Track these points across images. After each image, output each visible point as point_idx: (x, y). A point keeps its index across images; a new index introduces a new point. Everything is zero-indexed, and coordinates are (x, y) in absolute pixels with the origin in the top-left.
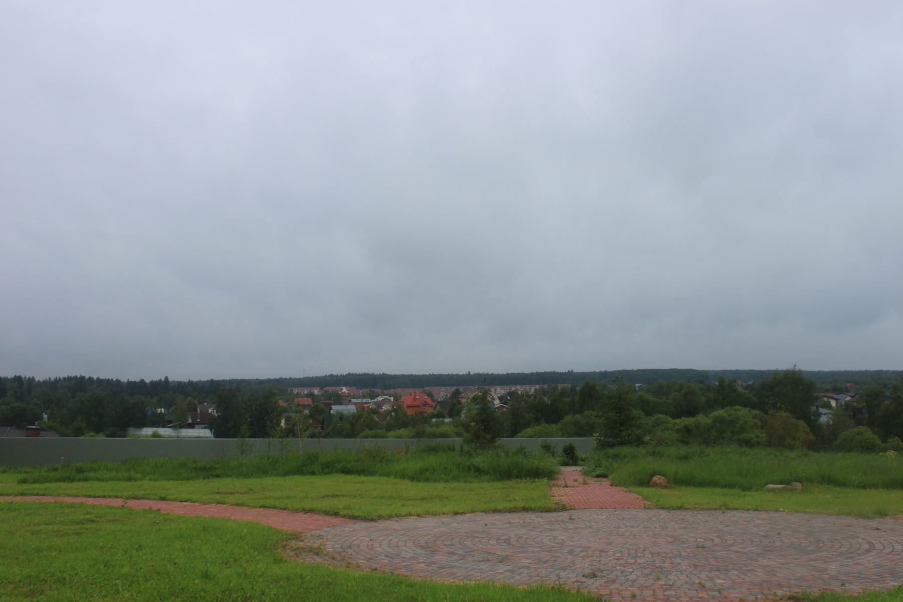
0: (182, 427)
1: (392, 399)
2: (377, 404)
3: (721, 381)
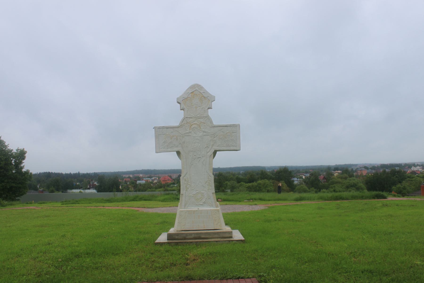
0: (86, 189)
2: (152, 180)
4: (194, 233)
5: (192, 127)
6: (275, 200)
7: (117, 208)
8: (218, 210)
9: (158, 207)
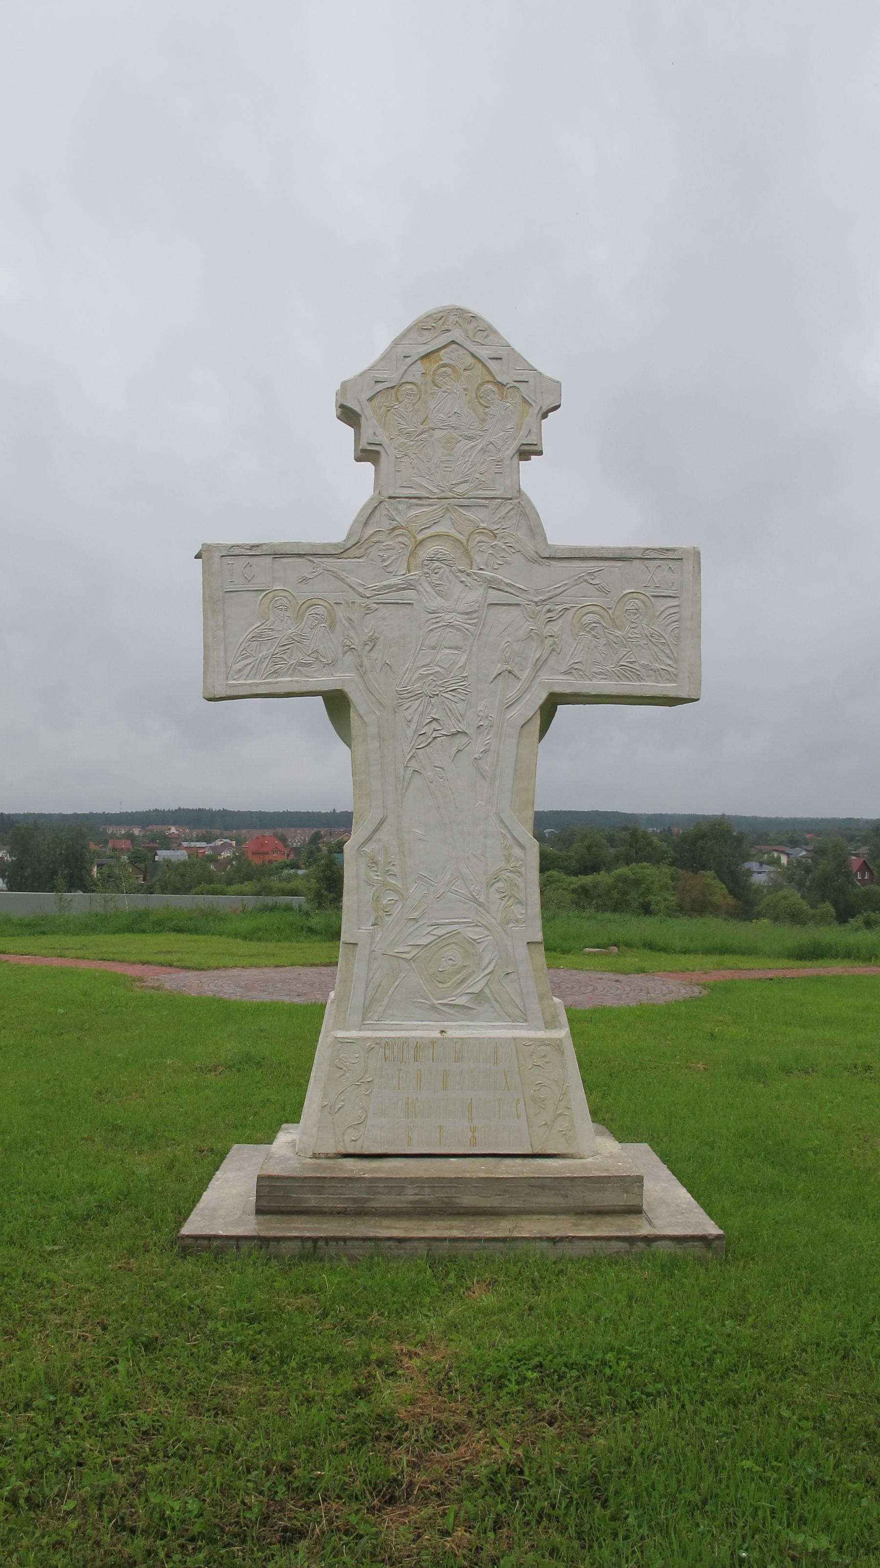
1: (234, 843)
3: (634, 834)
4: (413, 1181)
5: (425, 553)
6: (708, 952)
7: (56, 962)
8: (557, 1046)
9: (226, 967)
